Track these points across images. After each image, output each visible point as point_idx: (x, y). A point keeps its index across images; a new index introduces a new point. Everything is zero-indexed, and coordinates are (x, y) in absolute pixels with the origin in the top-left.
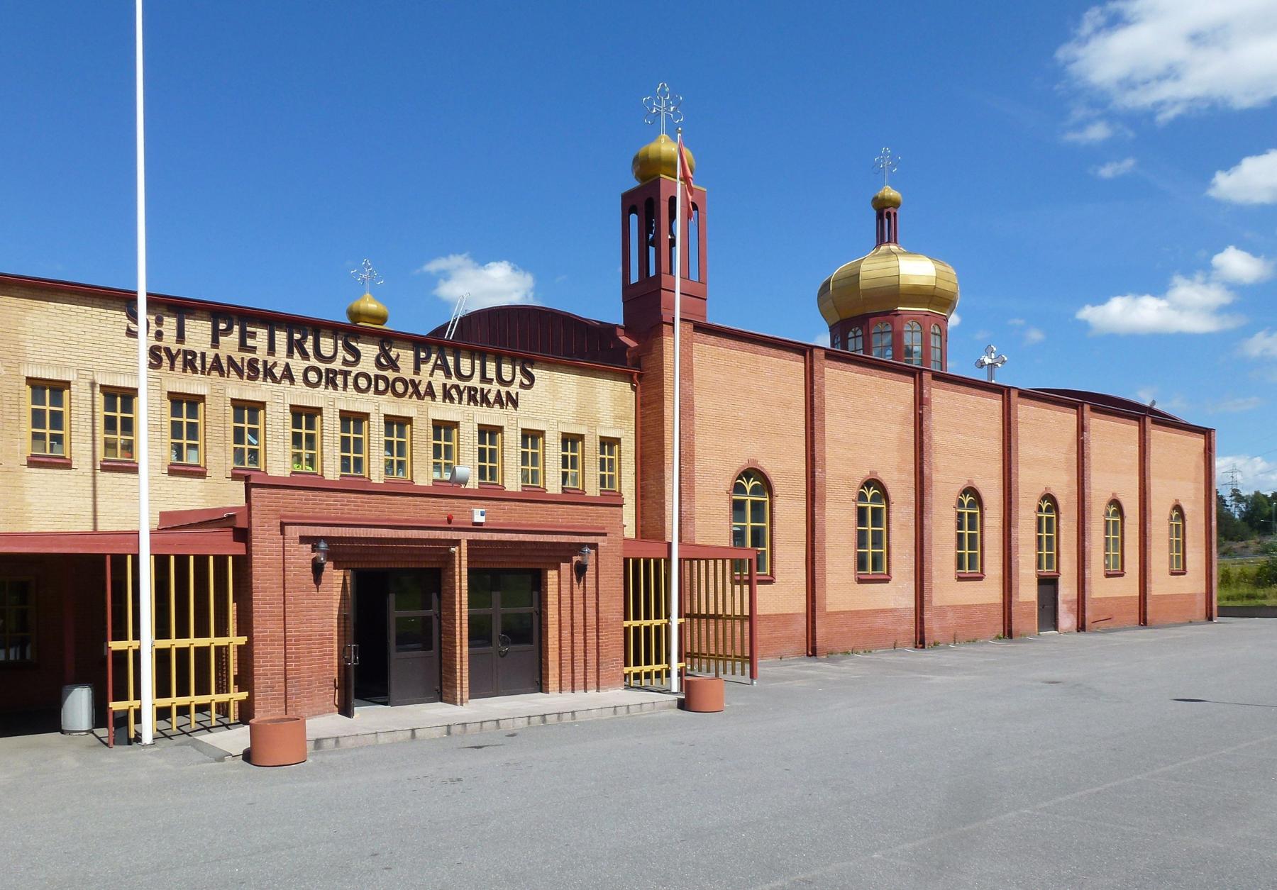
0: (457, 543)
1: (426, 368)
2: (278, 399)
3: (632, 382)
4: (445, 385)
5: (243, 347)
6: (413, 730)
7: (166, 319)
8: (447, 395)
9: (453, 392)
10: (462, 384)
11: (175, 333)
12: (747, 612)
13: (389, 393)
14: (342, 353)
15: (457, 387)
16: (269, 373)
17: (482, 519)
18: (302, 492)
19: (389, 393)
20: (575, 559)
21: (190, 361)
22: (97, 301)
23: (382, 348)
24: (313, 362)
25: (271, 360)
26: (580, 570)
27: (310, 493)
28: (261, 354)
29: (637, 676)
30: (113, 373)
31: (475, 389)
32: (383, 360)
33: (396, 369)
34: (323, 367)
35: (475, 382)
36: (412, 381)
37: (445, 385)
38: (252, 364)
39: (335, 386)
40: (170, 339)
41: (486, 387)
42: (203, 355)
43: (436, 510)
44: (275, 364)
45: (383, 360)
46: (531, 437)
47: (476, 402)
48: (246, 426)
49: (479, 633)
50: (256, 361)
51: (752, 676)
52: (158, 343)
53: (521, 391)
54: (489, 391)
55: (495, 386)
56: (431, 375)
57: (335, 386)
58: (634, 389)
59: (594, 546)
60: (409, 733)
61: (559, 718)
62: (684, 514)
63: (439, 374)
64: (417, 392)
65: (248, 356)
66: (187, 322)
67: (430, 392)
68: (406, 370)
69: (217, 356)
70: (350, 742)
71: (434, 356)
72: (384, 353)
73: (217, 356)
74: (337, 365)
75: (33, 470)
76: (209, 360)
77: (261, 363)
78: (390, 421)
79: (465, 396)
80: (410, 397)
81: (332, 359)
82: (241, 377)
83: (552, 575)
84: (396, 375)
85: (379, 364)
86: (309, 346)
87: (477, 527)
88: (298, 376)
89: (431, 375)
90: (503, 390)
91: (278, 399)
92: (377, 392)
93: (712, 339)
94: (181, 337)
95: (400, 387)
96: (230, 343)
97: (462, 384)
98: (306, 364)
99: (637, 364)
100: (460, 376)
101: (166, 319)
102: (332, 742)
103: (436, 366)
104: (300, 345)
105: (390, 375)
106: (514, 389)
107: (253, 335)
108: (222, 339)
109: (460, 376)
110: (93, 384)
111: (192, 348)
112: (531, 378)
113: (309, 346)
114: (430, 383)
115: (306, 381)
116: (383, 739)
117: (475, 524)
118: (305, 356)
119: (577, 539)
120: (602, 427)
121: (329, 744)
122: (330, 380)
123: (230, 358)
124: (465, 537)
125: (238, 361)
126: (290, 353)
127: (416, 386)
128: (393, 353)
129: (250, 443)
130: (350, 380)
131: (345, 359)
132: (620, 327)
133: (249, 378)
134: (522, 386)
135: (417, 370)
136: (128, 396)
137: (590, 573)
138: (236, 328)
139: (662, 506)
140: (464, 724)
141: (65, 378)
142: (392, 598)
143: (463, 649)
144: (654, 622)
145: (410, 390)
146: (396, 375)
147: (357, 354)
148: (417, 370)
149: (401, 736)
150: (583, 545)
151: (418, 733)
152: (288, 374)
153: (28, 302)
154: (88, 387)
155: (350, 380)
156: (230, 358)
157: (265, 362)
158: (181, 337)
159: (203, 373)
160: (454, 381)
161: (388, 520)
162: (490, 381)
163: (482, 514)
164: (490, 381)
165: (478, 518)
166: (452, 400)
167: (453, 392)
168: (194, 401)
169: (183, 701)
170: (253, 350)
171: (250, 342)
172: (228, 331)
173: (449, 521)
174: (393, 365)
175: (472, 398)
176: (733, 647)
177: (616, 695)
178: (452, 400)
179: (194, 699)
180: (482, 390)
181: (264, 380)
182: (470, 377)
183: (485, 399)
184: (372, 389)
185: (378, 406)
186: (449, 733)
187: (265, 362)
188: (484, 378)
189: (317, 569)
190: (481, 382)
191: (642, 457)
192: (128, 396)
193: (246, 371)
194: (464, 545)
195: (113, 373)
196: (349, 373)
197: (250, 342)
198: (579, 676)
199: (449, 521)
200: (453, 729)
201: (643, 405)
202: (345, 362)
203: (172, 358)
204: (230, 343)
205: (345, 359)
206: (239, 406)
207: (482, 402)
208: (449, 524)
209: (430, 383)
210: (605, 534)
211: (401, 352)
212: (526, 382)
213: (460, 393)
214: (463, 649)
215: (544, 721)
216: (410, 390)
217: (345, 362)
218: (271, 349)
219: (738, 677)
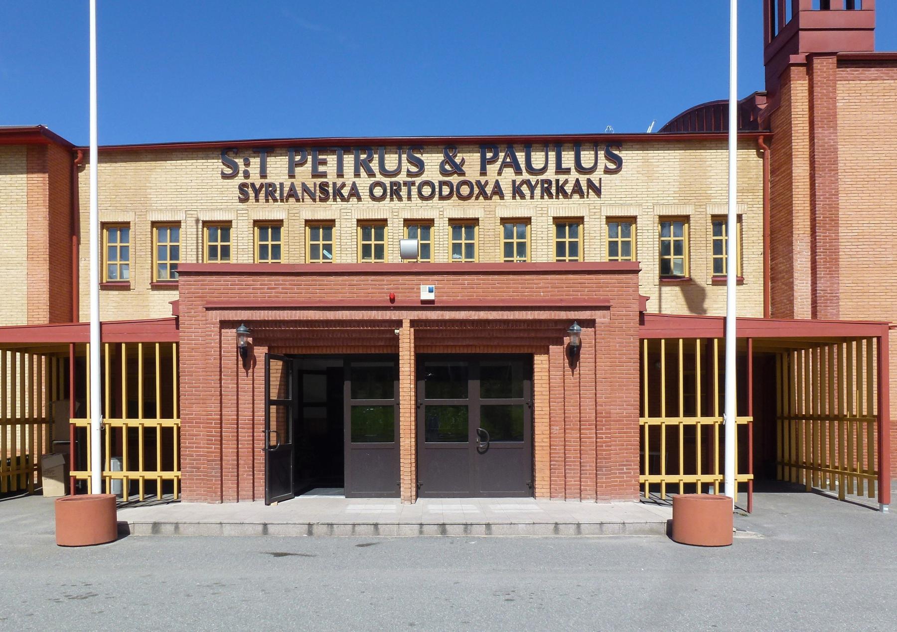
0: (399, 323)
1: (492, 169)
2: (346, 216)
3: (758, 148)
4: (514, 182)
5: (316, 174)
6: (265, 525)
7: (252, 160)
8: (517, 191)
9: (525, 189)
10: (533, 179)
11: (258, 171)
12: (875, 413)
13: (455, 197)
14: (406, 165)
15: (528, 182)
16: (338, 193)
17: (431, 297)
18: (228, 278)
19: (455, 197)
20: (567, 340)
21: (270, 192)
22: (200, 154)
23: (447, 155)
24: (379, 178)
25: (339, 182)
26: (573, 354)
27: (236, 278)
28: (331, 178)
29: (655, 488)
30: (212, 210)
31: (549, 182)
32: (447, 167)
33: (463, 174)
34: (387, 181)
35: (550, 174)
36: (478, 182)
37: (514, 182)
38: (323, 187)
39: (400, 199)
40: (255, 178)
41: (562, 178)
42: (282, 185)
43: (375, 290)
44: (343, 185)
45: (447, 167)
46: (622, 223)
47: (550, 196)
48: (321, 242)
49: (431, 427)
50: (327, 184)
51: (880, 500)
52: (246, 181)
53: (606, 178)
54: (566, 182)
55: (574, 175)
56: (500, 174)
57: (400, 199)
58: (761, 155)
59: (591, 323)
60: (260, 528)
61: (465, 530)
62: (820, 293)
63: (509, 173)
64: (483, 192)
65: (319, 181)
66: (269, 159)
67: (498, 191)
68: (472, 172)
69: (292, 184)
70: (191, 530)
71: (502, 155)
72: (449, 160)
73: (292, 184)
74: (402, 178)
75: (155, 292)
76: (286, 189)
77: (331, 186)
78: (456, 224)
79: (538, 191)
80: (477, 198)
81: (397, 173)
82: (314, 200)
83: (540, 362)
84: (462, 178)
85: (444, 172)
86: (375, 165)
87: (428, 305)
88: (364, 192)
89: (500, 174)
90: (583, 179)
91: (346, 216)
92: (442, 198)
93: (873, 72)
94: (263, 175)
95: (465, 190)
96: (304, 173)
97: (533, 179)
98: (373, 180)
99: (768, 126)
100: (531, 170)
101: (252, 160)
102: (171, 528)
103: (505, 165)
104: (366, 165)
105: (455, 179)
106: (594, 177)
107: (324, 163)
108: (298, 170)
109: (531, 170)
110: (197, 221)
111: (273, 181)
112: (618, 162)
113: (375, 165)
114: (497, 182)
115: (373, 197)
116: (228, 531)
117: (423, 302)
118: (371, 174)
119: (572, 315)
120: (715, 204)
121: (168, 529)
122: (395, 192)
123: (303, 184)
124: (407, 317)
125: (310, 186)
126: (357, 174)
127: (482, 187)
128: (458, 160)
129: (325, 257)
130: (414, 190)
131: (408, 171)
132: (762, 95)
133: (321, 200)
134: (607, 171)
135: (483, 172)
136: (225, 227)
137: (585, 354)
138: (310, 158)
139: (790, 286)
140: (331, 525)
141: (176, 218)
142: (347, 386)
143: (407, 441)
144: (699, 420)
145: (476, 191)
146: (462, 178)
147: (420, 164)
148: (483, 172)
149: (250, 530)
150: (571, 322)
151: (271, 529)
152: (355, 193)
153: (153, 163)
154: (194, 223)
155: (414, 190)
156: (303, 184)
157: (334, 184)
158: (263, 175)
159: (282, 201)
160: (526, 176)
161: (320, 302)
162: (567, 171)
163: (431, 291)
164: (567, 171)
165: (426, 295)
166: (523, 196)
167: (525, 189)
168: (276, 226)
169: (673, 479)
170: (324, 175)
171: (321, 169)
172: (302, 163)
173: (392, 300)
174: (458, 170)
175: (546, 191)
176: (860, 459)
177: (254, 510)
178: (523, 196)
179: (682, 478)
180: (557, 181)
181: (335, 200)
182: (543, 170)
183: (561, 190)
184: (437, 196)
185: (441, 212)
186: (310, 533)
187: (334, 184)
188: (560, 170)
189: (246, 354)
190: (557, 173)
191: (772, 233)
192: (225, 227)
193: (318, 193)
194: (406, 324)
195: (212, 210)
196: (413, 184)
197: (321, 169)
198: (573, 481)
199: (392, 300)
200: (315, 529)
201: (773, 172)
202: (409, 174)
203: (257, 192)
204: (304, 173)
205: (408, 171)
206: (313, 225)
207: (557, 194)
208: (392, 304)
209: (497, 182)
210: (607, 308)
211: (467, 156)
212: (612, 166)
213: (532, 189)
214: (407, 441)
215: (310, 533)
216: (476, 191)
217: (409, 174)
218: (340, 175)
219: (865, 499)
